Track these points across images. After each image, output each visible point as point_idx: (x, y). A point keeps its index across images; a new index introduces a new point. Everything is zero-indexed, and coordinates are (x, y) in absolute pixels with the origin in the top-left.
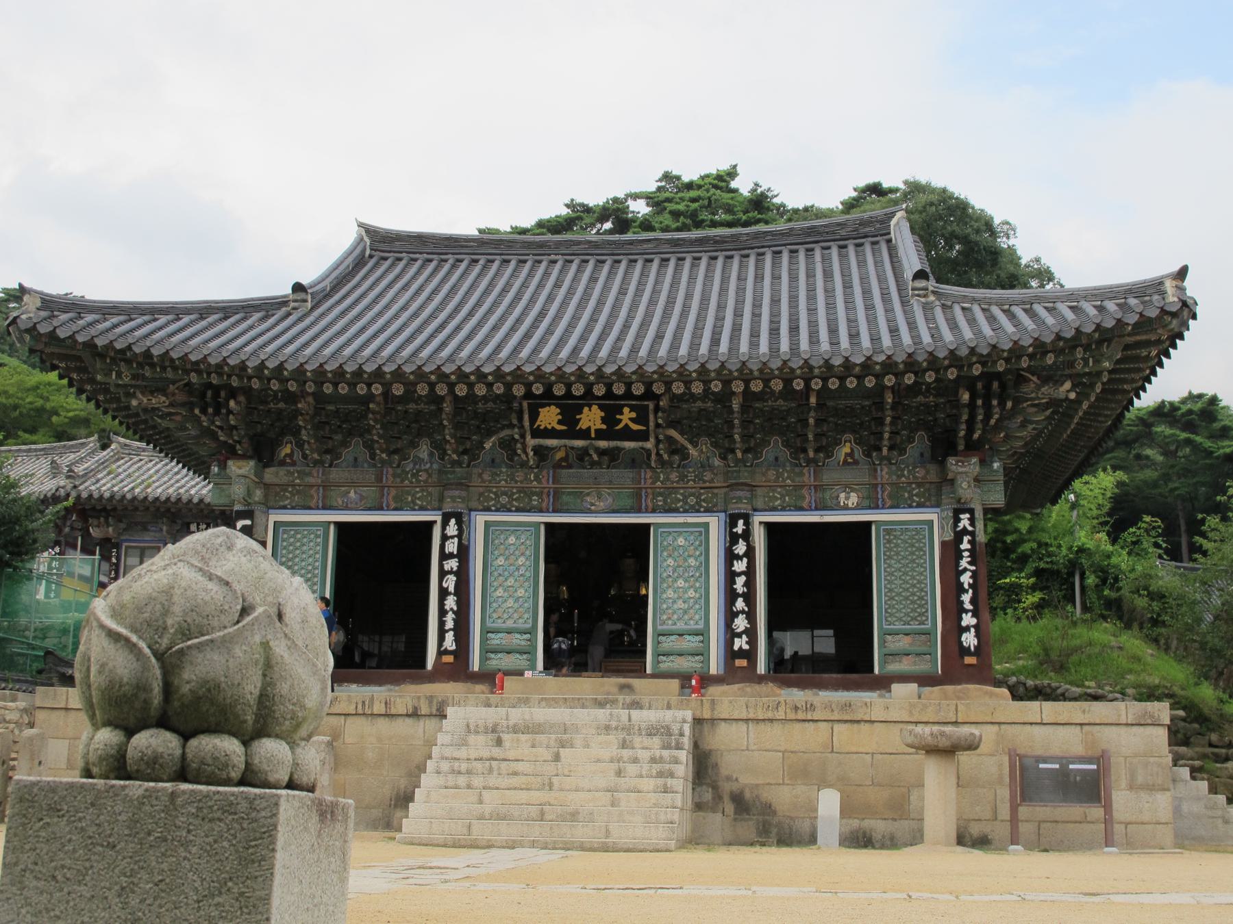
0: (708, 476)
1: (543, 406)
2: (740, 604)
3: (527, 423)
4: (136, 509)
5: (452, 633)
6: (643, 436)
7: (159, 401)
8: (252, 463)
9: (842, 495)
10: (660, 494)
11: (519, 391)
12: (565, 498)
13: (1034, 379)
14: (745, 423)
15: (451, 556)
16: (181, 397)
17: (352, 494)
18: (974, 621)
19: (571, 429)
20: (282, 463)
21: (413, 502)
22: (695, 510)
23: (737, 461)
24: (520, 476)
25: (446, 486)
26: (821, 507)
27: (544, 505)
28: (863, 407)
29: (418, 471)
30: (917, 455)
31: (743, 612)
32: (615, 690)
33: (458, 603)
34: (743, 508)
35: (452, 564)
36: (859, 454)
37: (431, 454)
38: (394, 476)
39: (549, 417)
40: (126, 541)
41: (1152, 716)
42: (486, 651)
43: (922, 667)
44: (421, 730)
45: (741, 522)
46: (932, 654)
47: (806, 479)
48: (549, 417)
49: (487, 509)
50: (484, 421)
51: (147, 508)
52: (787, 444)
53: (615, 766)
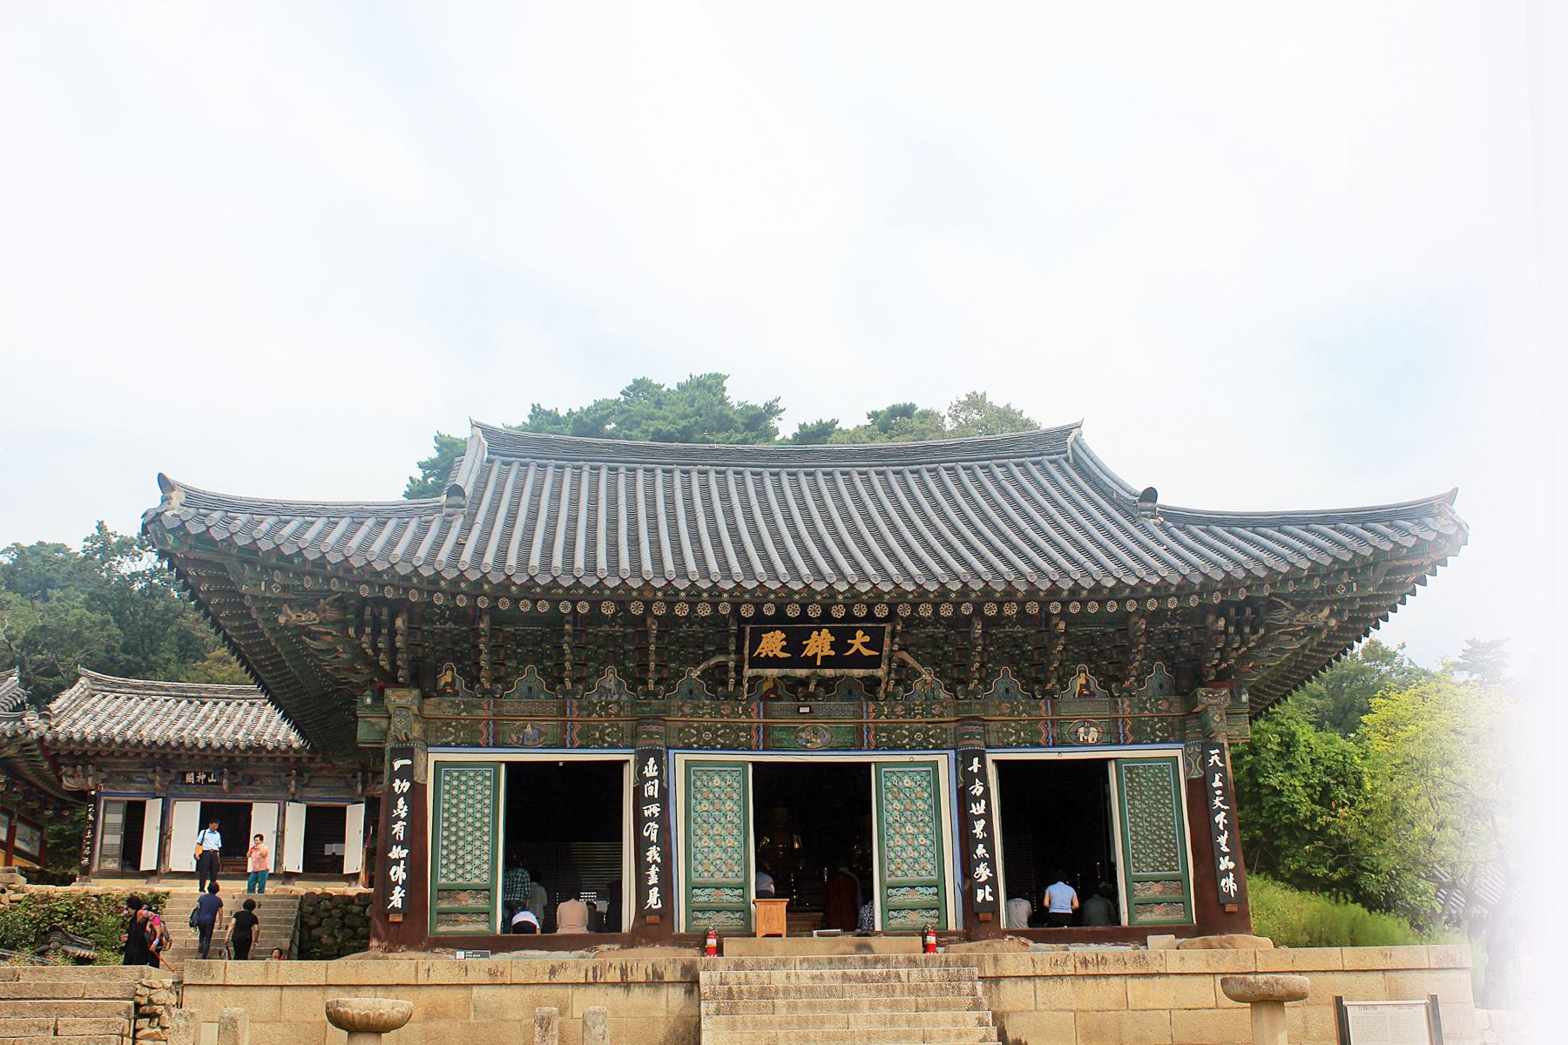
1: (768, 631)
3: (746, 652)
4: (125, 754)
5: (656, 889)
6: (874, 662)
8: (416, 692)
9: (1082, 730)
10: (883, 730)
11: (1055, 608)
13: (1288, 605)
14: (493, 650)
15: (651, 800)
16: (332, 614)
17: (529, 729)
18: (1232, 865)
19: (795, 654)
20: (442, 693)
23: (648, 694)
25: (641, 721)
26: (1059, 743)
27: (754, 742)
29: (608, 703)
30: (1156, 686)
31: (984, 859)
33: (661, 854)
34: (978, 744)
35: (654, 809)
36: (1094, 684)
37: (619, 684)
38: (579, 708)
39: (772, 644)
40: (107, 794)
42: (692, 909)
43: (1176, 917)
44: (663, 1000)
45: (976, 760)
46: (1185, 903)
48: (772, 644)
49: (688, 747)
50: (682, 648)
52: (1019, 674)
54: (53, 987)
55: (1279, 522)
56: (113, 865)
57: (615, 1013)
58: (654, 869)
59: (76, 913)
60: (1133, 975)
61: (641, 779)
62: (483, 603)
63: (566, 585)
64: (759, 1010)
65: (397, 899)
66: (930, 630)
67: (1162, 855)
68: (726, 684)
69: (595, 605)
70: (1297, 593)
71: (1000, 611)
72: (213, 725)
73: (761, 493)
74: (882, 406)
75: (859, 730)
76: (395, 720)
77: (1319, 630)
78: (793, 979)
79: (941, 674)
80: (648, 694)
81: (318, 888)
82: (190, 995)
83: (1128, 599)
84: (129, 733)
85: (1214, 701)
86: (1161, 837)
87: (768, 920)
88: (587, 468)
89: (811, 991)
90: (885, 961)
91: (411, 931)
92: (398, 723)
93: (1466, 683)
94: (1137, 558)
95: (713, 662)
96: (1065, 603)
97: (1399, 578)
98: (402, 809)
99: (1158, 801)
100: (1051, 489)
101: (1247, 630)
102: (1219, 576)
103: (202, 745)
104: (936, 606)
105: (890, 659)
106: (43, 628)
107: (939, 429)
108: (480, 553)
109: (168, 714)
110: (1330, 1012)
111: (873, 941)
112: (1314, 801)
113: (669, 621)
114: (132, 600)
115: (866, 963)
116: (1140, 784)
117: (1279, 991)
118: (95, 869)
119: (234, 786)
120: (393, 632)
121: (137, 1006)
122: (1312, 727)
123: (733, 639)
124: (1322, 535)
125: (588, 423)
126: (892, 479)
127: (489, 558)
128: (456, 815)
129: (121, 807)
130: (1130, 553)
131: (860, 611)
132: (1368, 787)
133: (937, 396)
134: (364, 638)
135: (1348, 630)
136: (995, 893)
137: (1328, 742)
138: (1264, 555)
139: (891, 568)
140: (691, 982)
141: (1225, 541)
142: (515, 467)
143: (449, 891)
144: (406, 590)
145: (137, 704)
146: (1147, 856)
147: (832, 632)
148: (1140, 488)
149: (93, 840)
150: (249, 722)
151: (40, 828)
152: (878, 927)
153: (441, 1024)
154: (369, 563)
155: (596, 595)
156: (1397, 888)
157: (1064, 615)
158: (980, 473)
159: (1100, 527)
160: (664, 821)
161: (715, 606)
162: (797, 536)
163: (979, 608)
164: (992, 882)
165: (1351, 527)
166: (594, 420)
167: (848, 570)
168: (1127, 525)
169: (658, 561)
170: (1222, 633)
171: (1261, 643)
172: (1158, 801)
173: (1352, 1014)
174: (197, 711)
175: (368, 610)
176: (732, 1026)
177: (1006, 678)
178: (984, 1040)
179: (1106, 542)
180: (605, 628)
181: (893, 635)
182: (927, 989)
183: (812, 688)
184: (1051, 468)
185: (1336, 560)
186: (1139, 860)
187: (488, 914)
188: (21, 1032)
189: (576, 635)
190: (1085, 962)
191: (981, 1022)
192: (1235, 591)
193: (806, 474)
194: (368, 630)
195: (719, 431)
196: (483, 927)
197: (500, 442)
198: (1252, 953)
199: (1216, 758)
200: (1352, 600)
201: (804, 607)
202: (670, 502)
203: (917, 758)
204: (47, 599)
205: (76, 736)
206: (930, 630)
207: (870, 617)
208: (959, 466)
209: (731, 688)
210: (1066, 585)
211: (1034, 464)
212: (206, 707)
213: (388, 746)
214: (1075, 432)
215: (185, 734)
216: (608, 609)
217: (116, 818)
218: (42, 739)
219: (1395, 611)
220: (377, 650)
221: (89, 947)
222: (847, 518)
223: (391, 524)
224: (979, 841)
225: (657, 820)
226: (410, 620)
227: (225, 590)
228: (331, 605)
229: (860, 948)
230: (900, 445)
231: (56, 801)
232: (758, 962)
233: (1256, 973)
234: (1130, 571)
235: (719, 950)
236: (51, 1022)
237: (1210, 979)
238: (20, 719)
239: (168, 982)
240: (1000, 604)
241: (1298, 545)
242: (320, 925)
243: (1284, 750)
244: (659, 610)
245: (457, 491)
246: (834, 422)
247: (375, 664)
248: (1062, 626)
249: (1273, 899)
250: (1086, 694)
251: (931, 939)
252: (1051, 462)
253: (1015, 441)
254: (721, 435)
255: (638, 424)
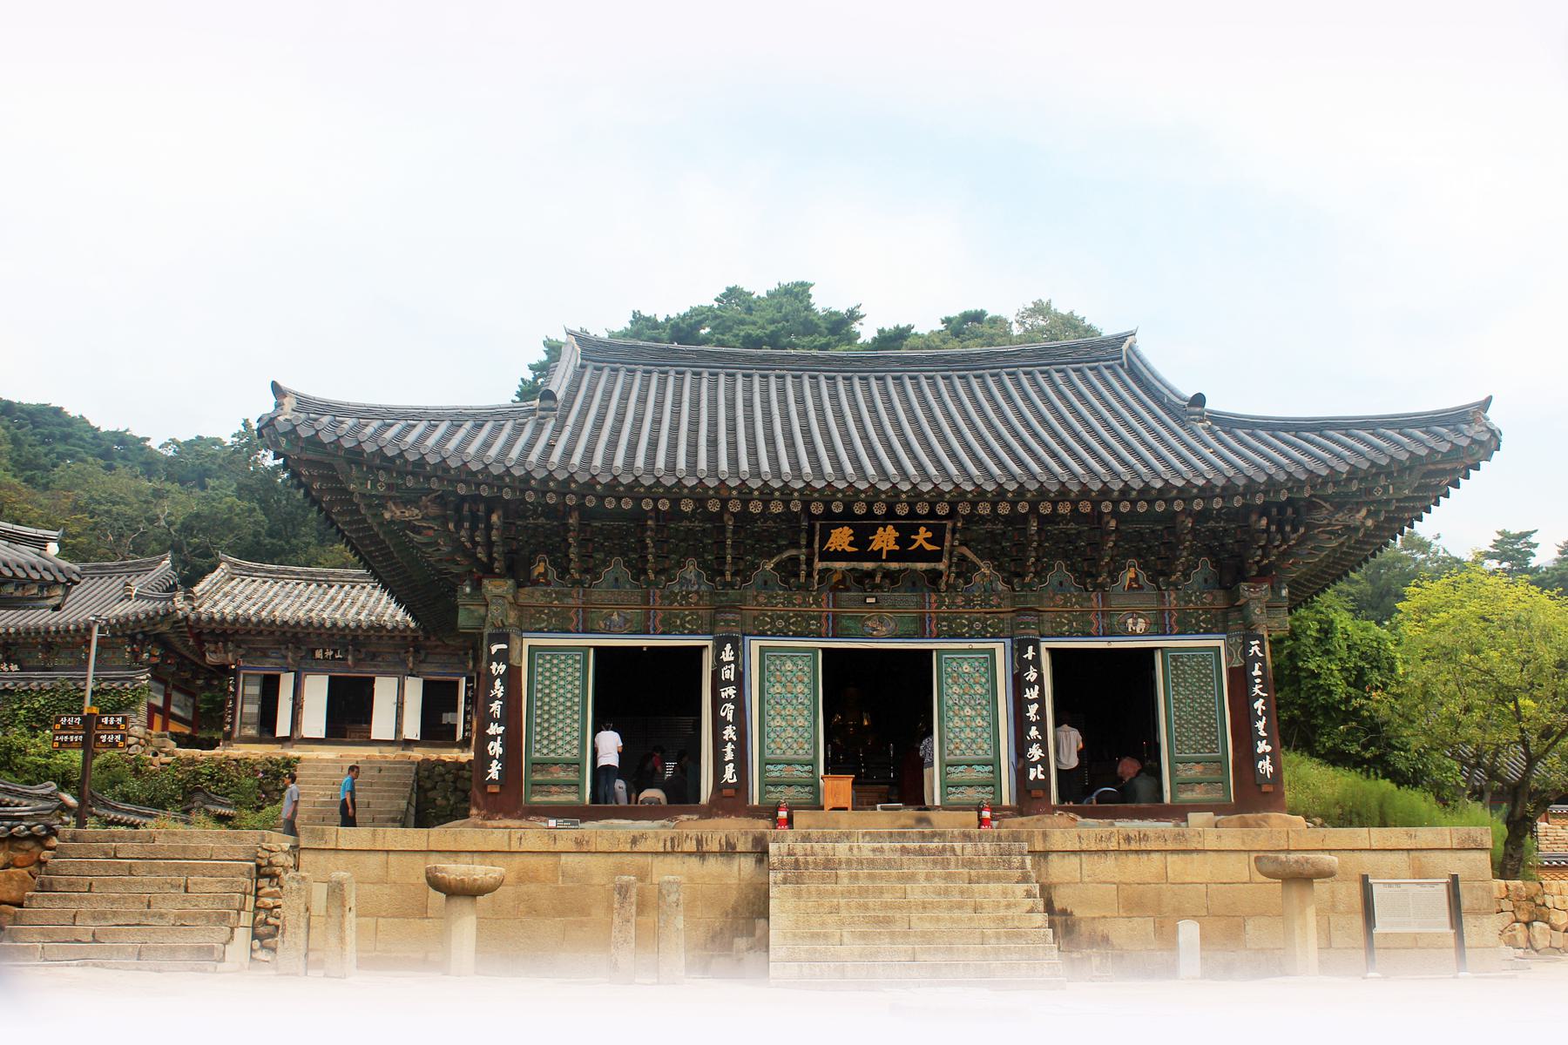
0: (994, 600)
2: (1034, 732)
3: (816, 546)
4: (260, 633)
6: (936, 557)
7: (412, 514)
8: (510, 582)
10: (944, 619)
11: (1106, 507)
12: (845, 623)
14: (582, 543)
15: (728, 683)
16: (434, 510)
17: (615, 617)
18: (1268, 749)
19: (862, 548)
20: (535, 583)
21: (682, 625)
22: (981, 635)
23: (726, 585)
24: (797, 599)
25: (718, 610)
26: (1109, 633)
28: (1153, 531)
30: (1201, 580)
31: (1036, 741)
32: (911, 822)
34: (1032, 633)
35: (730, 692)
37: (699, 575)
38: (662, 597)
39: (841, 538)
40: (246, 668)
41: (1475, 841)
42: (764, 783)
43: (1215, 796)
44: (736, 868)
45: (1030, 648)
46: (1225, 782)
47: (1094, 604)
48: (841, 538)
49: (763, 634)
50: (758, 541)
51: (272, 633)
52: (1072, 568)
53: (154, 910)
54: (184, 849)
55: (1321, 426)
56: (251, 732)
57: (691, 880)
58: (730, 747)
59: (220, 775)
60: (1173, 851)
61: (719, 664)
62: (571, 500)
63: (647, 483)
64: (823, 880)
65: (494, 771)
66: (989, 526)
67: (1203, 738)
68: (797, 576)
69: (675, 502)
70: (1336, 494)
71: (1054, 509)
72: (339, 607)
73: (834, 397)
74: (955, 312)
75: (922, 619)
76: (492, 608)
77: (1356, 529)
78: (855, 851)
79: (999, 568)
80: (726, 585)
81: (433, 754)
82: (305, 858)
83: (1176, 499)
84: (264, 614)
85: (1255, 595)
86: (1203, 722)
87: (835, 795)
88: (672, 373)
89: (872, 862)
90: (942, 836)
91: (508, 800)
92: (495, 611)
93: (1494, 573)
94: (1185, 461)
95: (785, 555)
96: (1116, 503)
97: (1434, 481)
98: (498, 689)
99: (1201, 688)
100: (1106, 393)
101: (1288, 528)
102: (1262, 479)
103: (328, 624)
104: (994, 505)
105: (951, 554)
106: (197, 516)
107: (1007, 334)
108: (568, 453)
109: (299, 596)
110: (1356, 888)
111: (933, 815)
112: (1349, 684)
113: (744, 517)
114: (276, 490)
115: (923, 836)
116: (1184, 672)
117: (1308, 869)
118: (236, 734)
119: (357, 662)
120: (489, 527)
121: (259, 867)
122: (1351, 615)
123: (804, 535)
124: (1362, 440)
125: (684, 329)
126: (957, 382)
127: (576, 459)
128: (548, 695)
129: (258, 680)
130: (1179, 455)
131: (923, 509)
132: (1400, 671)
133: (1007, 303)
134: (463, 533)
135: (1384, 529)
136: (1046, 772)
137: (1365, 629)
138: (1305, 459)
139: (952, 469)
140: (760, 851)
141: (1269, 445)
142: (606, 372)
143: (542, 765)
144: (500, 489)
145: (271, 587)
146: (1189, 738)
147: (896, 528)
148: (1190, 394)
149: (234, 709)
150: (371, 604)
151: (192, 695)
152: (937, 802)
153: (533, 887)
154: (465, 464)
155: (675, 493)
156: (1425, 765)
157: (1115, 513)
158: (1040, 378)
159: (1151, 430)
160: (740, 702)
161: (786, 503)
162: (865, 438)
163: (1034, 506)
164: (1044, 761)
165: (1390, 432)
166: (690, 325)
167: (911, 470)
168: (1177, 428)
169: (734, 460)
170: (1264, 531)
171: (1302, 541)
172: (1201, 688)
173: (1377, 891)
174: (325, 593)
175: (466, 507)
176: (798, 895)
177: (1059, 572)
178: (1031, 911)
179: (1156, 444)
180: (686, 523)
181: (954, 531)
182: (979, 863)
183: (878, 580)
184: (1107, 373)
185: (1373, 464)
186: (1182, 743)
187: (578, 786)
188: (156, 889)
189: (659, 529)
190: (1128, 839)
191: (1029, 894)
192: (1277, 492)
193: (877, 378)
194: (467, 525)
195: (804, 335)
196: (573, 798)
197: (595, 352)
198: (1284, 831)
199: (1256, 648)
200: (1388, 501)
201: (870, 505)
202: (749, 404)
203: (976, 646)
204: (204, 487)
205: (217, 616)
206: (989, 526)
207: (932, 514)
208: (1020, 372)
209: (802, 580)
210: (1117, 486)
211: (1091, 369)
212: (333, 591)
213: (487, 631)
214: (1130, 340)
215: (313, 614)
216: (687, 506)
217: (254, 690)
218: (186, 618)
219: (1429, 511)
220: (475, 544)
221: (229, 806)
222: (914, 420)
223: (488, 427)
224: (1033, 724)
225: (733, 702)
226: (506, 516)
227: (331, 484)
228: (433, 501)
229: (920, 821)
230: (970, 351)
231: (200, 671)
232: (823, 835)
233: (1288, 851)
234: (1178, 473)
235: (789, 822)
236: (182, 880)
237: (1245, 856)
238: (171, 599)
239: (286, 846)
240: (1055, 503)
241: (1339, 449)
242: (434, 788)
243: (1322, 636)
244: (735, 507)
245: (550, 395)
246: (910, 328)
247: (472, 556)
248: (1113, 523)
249: (1313, 777)
250: (1135, 587)
251: (986, 814)
252: (1107, 367)
253: (1074, 348)
254: (808, 339)
255: (730, 328)
